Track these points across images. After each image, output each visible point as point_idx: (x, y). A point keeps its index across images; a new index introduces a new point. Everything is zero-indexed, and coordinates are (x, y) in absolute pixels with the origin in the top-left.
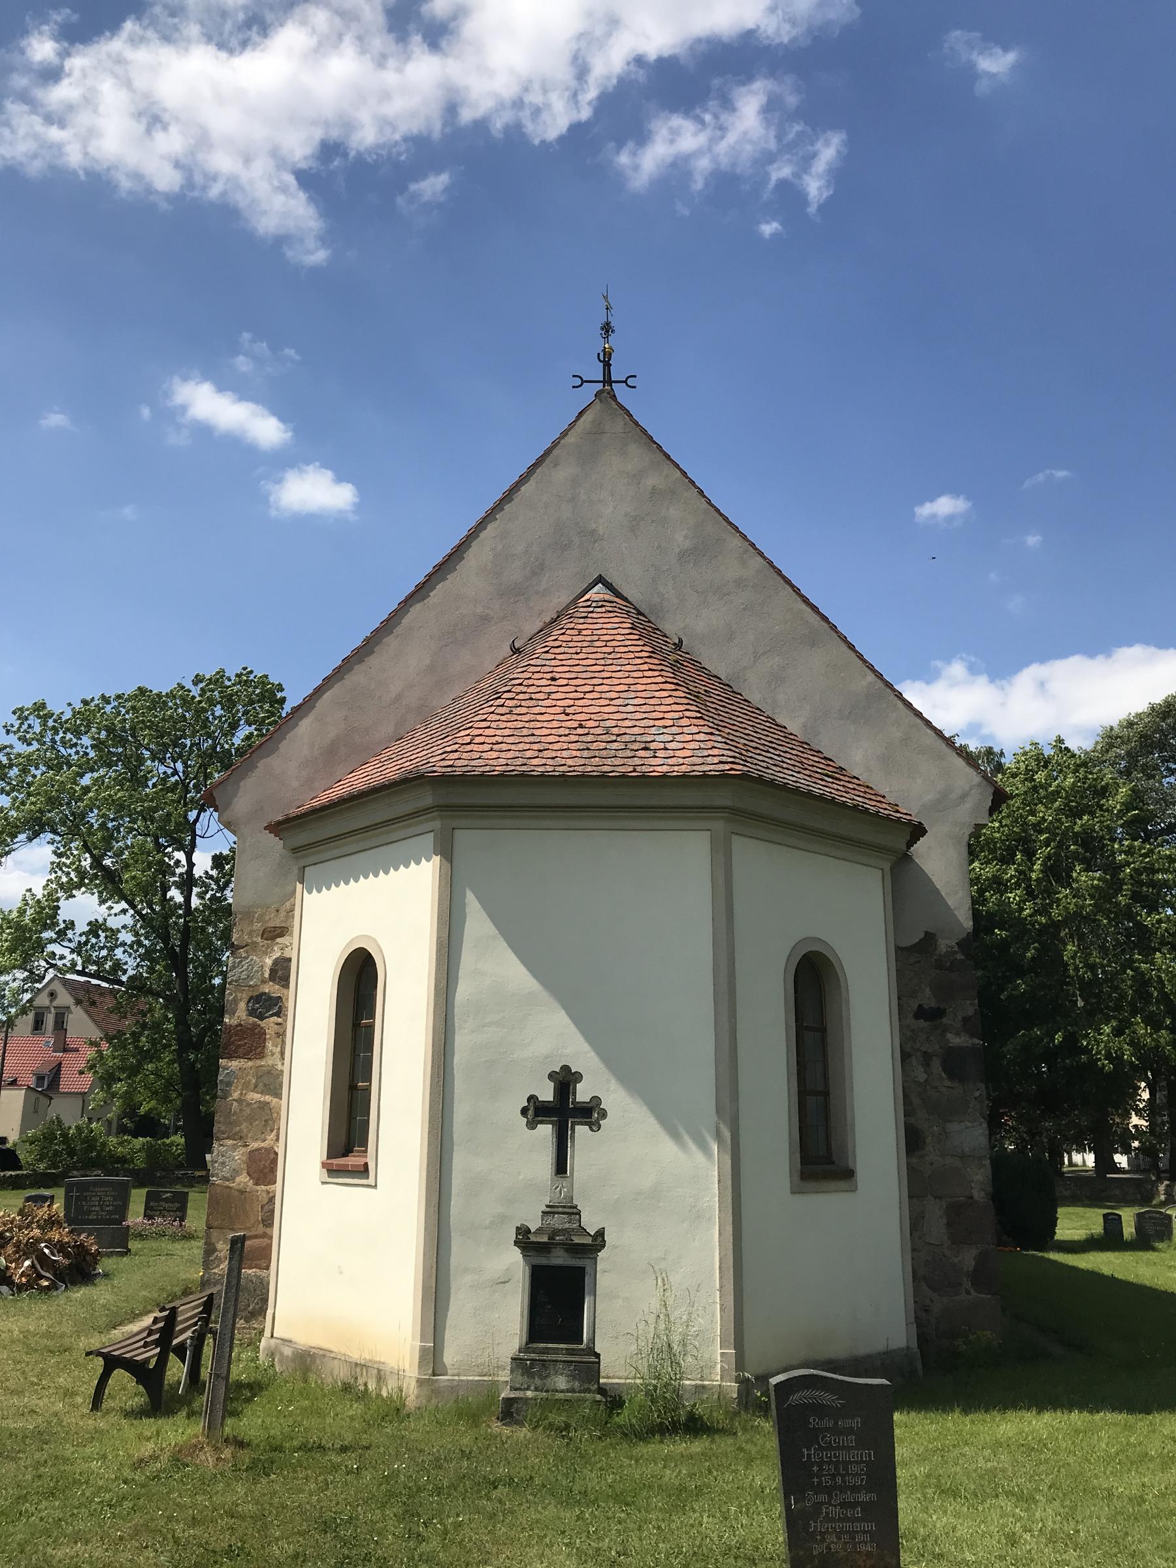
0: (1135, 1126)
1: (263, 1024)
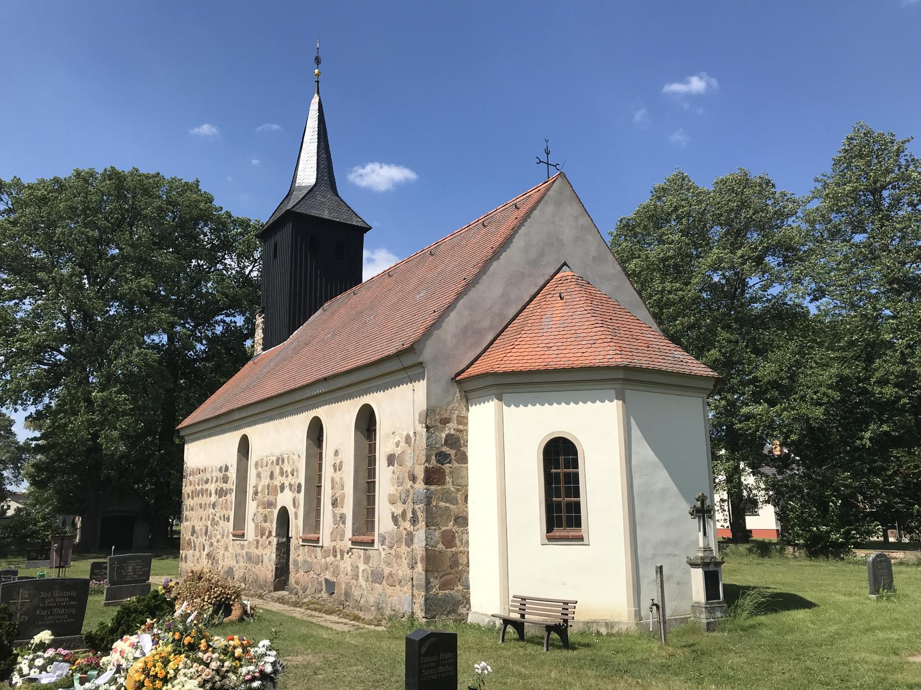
0: (9, 507)
1: (444, 467)
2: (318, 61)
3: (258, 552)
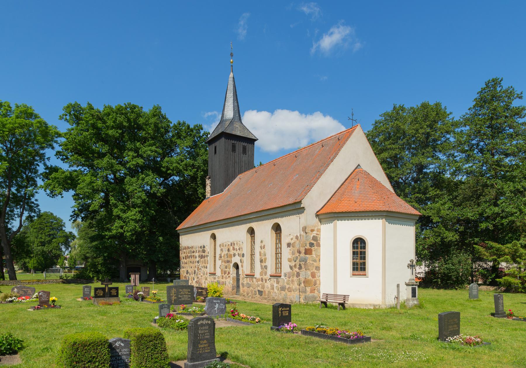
2: (232, 55)
3: (224, 280)
